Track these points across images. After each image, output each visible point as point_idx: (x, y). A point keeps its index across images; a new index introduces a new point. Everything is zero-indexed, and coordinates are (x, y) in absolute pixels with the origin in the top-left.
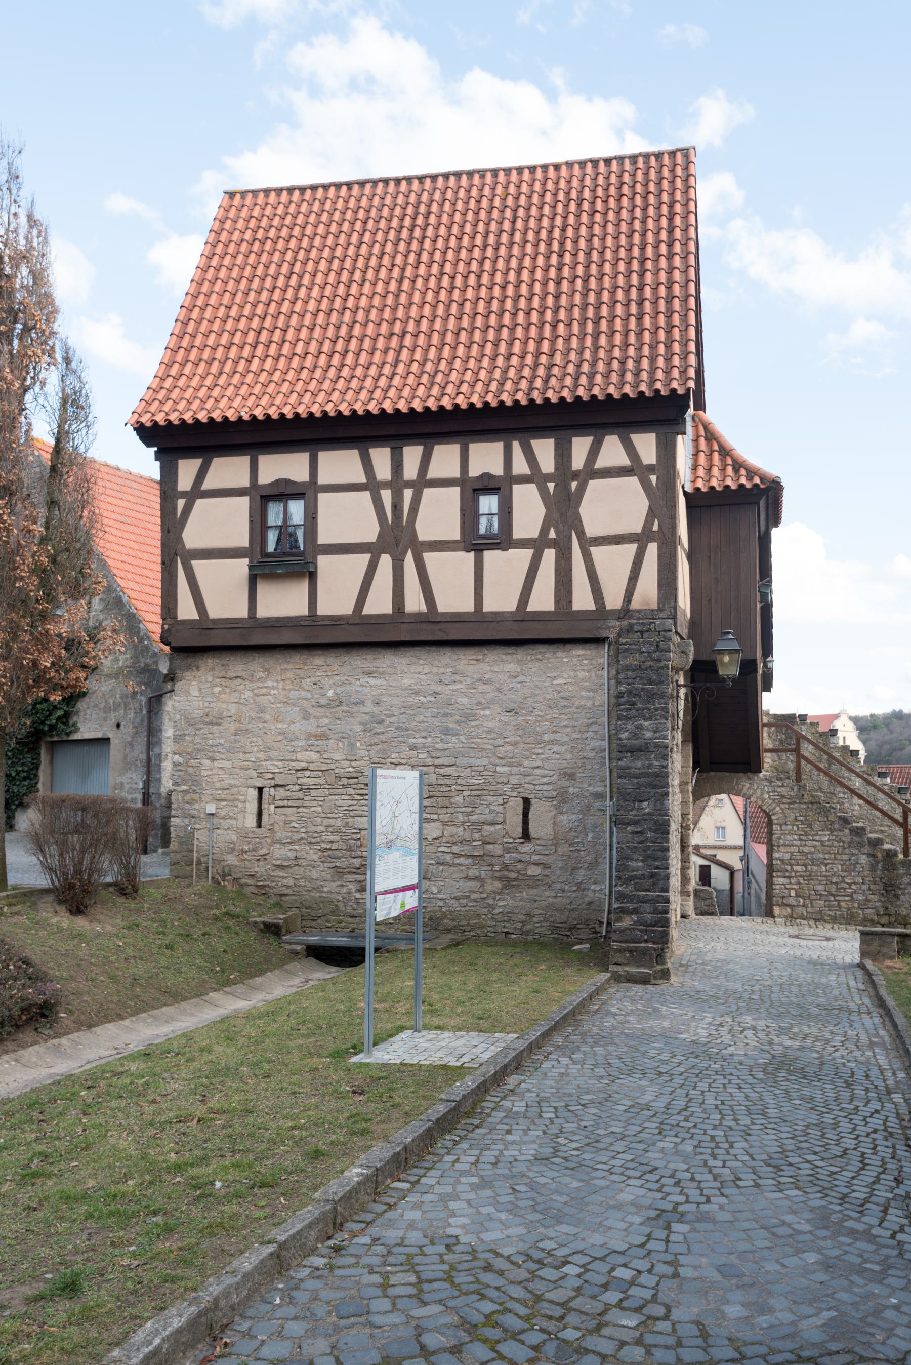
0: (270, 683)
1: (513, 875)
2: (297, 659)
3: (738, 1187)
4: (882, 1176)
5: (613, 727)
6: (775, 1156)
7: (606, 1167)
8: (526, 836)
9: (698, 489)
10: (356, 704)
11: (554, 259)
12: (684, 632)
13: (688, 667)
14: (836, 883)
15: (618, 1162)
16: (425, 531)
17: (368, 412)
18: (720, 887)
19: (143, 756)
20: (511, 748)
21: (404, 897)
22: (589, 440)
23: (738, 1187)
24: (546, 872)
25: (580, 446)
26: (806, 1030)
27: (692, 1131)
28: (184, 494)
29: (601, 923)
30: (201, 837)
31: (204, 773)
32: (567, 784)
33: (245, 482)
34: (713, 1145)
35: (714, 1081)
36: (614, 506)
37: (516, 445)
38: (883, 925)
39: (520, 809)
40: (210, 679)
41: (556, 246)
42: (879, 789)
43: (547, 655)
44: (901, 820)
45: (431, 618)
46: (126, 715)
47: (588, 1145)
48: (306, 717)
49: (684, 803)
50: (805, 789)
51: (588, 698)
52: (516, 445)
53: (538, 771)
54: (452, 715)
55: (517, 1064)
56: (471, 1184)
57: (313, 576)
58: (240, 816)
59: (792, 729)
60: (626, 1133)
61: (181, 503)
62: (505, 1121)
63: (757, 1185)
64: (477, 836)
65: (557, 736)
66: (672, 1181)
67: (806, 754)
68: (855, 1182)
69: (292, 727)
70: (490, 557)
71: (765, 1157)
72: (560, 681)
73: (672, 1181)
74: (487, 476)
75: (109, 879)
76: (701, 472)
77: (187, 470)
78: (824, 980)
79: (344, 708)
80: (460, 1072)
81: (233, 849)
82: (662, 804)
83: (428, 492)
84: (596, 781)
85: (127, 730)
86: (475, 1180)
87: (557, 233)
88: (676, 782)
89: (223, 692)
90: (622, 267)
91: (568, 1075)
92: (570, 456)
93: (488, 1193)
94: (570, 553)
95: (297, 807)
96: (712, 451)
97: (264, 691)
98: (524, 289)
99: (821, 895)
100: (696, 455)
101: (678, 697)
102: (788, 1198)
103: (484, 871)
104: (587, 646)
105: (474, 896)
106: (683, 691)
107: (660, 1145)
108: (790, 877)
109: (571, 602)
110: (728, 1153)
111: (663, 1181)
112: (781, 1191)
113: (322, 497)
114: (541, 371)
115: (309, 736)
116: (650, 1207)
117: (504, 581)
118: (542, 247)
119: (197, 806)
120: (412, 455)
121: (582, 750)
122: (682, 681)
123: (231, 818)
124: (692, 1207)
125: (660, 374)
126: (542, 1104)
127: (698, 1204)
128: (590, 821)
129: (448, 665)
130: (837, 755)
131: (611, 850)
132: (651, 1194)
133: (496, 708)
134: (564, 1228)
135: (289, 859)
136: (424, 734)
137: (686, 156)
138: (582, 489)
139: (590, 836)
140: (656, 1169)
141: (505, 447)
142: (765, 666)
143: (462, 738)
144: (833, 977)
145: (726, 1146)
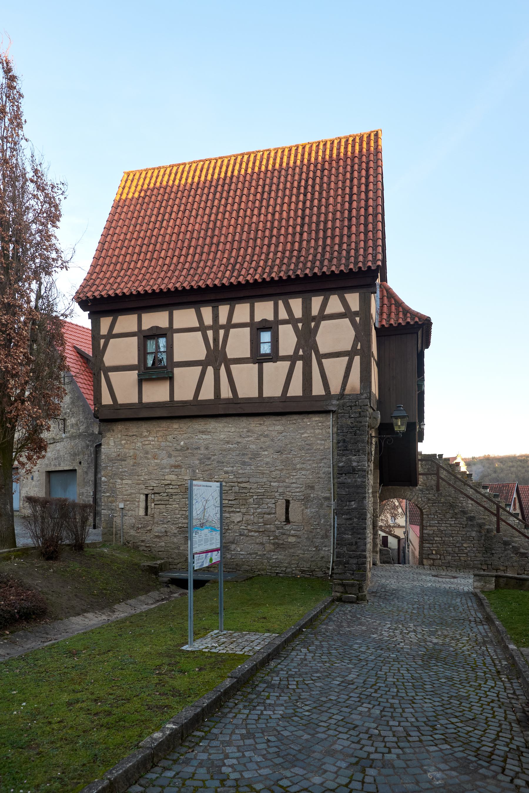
0: (150, 438)
1: (281, 542)
2: (164, 424)
3: (409, 741)
4: (500, 734)
5: (335, 460)
6: (431, 719)
7: (325, 724)
8: (287, 520)
9: (383, 326)
10: (196, 449)
11: (301, 197)
12: (375, 407)
13: (377, 427)
14: (458, 547)
15: (333, 721)
16: (231, 354)
17: (199, 287)
18: (393, 548)
19: (93, 479)
20: (279, 472)
21: (212, 555)
22: (321, 298)
23: (409, 741)
24: (298, 540)
25: (316, 302)
26: (445, 632)
27: (380, 699)
28: (103, 337)
29: (329, 569)
30: (118, 520)
31: (118, 486)
32: (310, 492)
33: (135, 329)
34: (392, 710)
35: (393, 665)
36: (337, 335)
37: (280, 303)
38: (484, 570)
39: (284, 506)
40: (120, 436)
41: (302, 190)
42: (483, 495)
43: (299, 421)
44: (495, 512)
45: (235, 400)
46: (83, 458)
47: (315, 708)
48: (170, 456)
49: (375, 503)
50: (441, 495)
51: (321, 444)
52: (280, 303)
53: (294, 485)
54: (247, 454)
55: (276, 653)
56: (241, 735)
57: (171, 379)
58: (137, 509)
59: (434, 462)
60: (339, 700)
61: (102, 341)
62: (266, 690)
63: (421, 741)
64: (261, 520)
65: (304, 466)
66: (367, 736)
67: (443, 476)
68: (483, 738)
69: (163, 462)
70: (266, 366)
71: (425, 719)
72: (306, 435)
73: (367, 736)
74: (264, 321)
75: (67, 542)
76: (385, 316)
77: (105, 323)
78: (454, 602)
79: (190, 451)
80: (242, 658)
81: (133, 527)
82: (363, 503)
83: (232, 331)
84: (325, 490)
85: (85, 465)
86: (244, 731)
87: (303, 183)
88: (370, 491)
89: (126, 443)
90: (339, 199)
91: (306, 660)
92: (311, 308)
93: (251, 741)
94: (311, 363)
95: (166, 505)
96: (391, 304)
97: (147, 443)
98: (285, 215)
99: (450, 553)
100: (382, 306)
101: (371, 443)
102: (441, 750)
103: (265, 539)
104: (321, 415)
105: (259, 553)
106: (374, 440)
107: (360, 709)
108: (432, 544)
109: (311, 391)
110: (402, 716)
111: (361, 736)
112: (436, 745)
113: (176, 336)
114: (294, 260)
115: (172, 466)
116: (352, 756)
117: (275, 380)
118: (295, 191)
119: (114, 504)
120: (224, 310)
121: (318, 473)
122: (373, 435)
123: (132, 510)
124: (378, 756)
125: (361, 258)
126: (290, 679)
127: (383, 753)
128: (322, 512)
129: (244, 428)
130: (460, 476)
131: (334, 528)
132: (353, 746)
133: (271, 451)
134: (297, 770)
135: (162, 533)
136: (231, 465)
137: (376, 135)
138: (317, 327)
139: (322, 521)
140: (357, 726)
141: (274, 304)
142: (420, 427)
143: (253, 467)
144: (458, 600)
145: (400, 710)
